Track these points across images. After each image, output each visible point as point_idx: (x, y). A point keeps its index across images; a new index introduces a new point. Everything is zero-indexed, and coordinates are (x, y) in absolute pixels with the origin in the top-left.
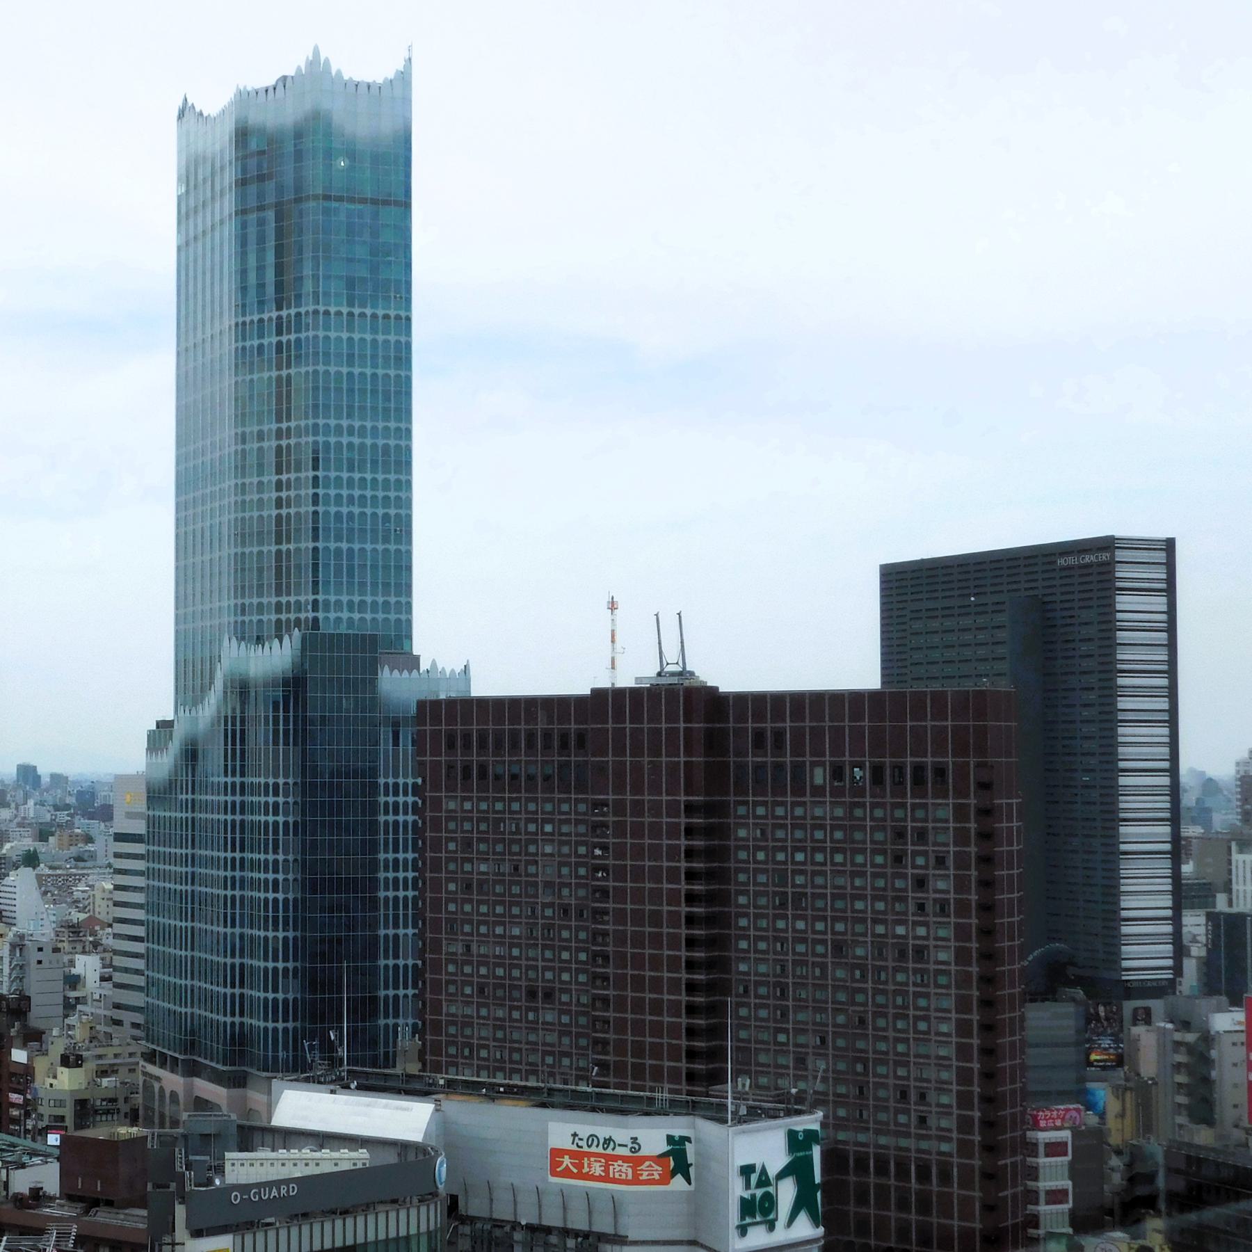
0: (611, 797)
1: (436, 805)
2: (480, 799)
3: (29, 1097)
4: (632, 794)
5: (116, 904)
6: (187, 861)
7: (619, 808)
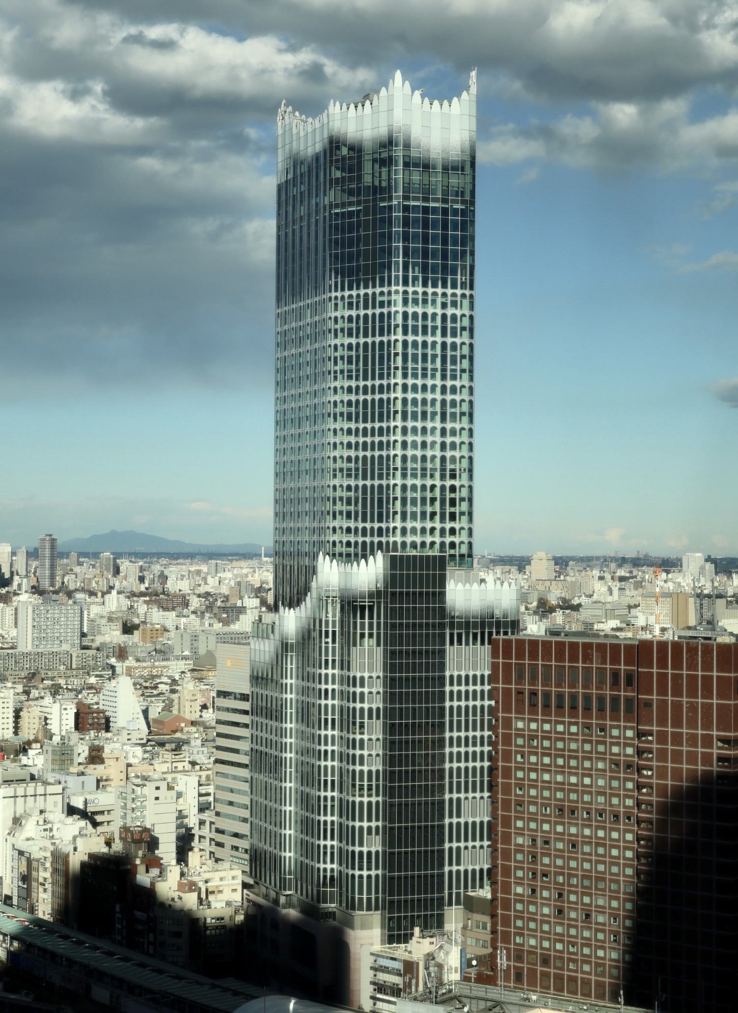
0: (655, 728)
1: (508, 723)
2: (544, 721)
3: (151, 915)
4: (672, 727)
5: (219, 748)
6: (325, 853)
7: (662, 737)
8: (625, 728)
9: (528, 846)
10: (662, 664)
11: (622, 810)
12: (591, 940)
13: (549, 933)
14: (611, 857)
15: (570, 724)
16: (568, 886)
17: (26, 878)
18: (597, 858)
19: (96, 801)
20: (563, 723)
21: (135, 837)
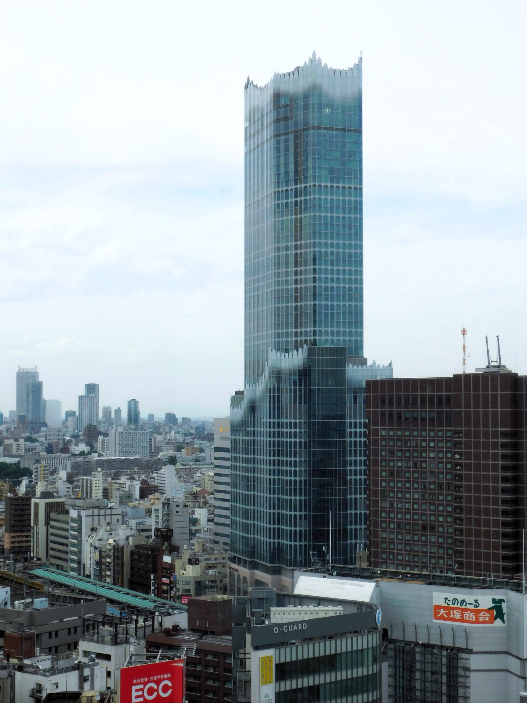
0: (463, 429)
1: (376, 432)
3: (172, 580)
9: (389, 508)
10: (467, 389)
11: (445, 481)
13: (402, 560)
14: (439, 511)
16: (413, 531)
17: (98, 563)
19: (144, 523)
21: (164, 534)
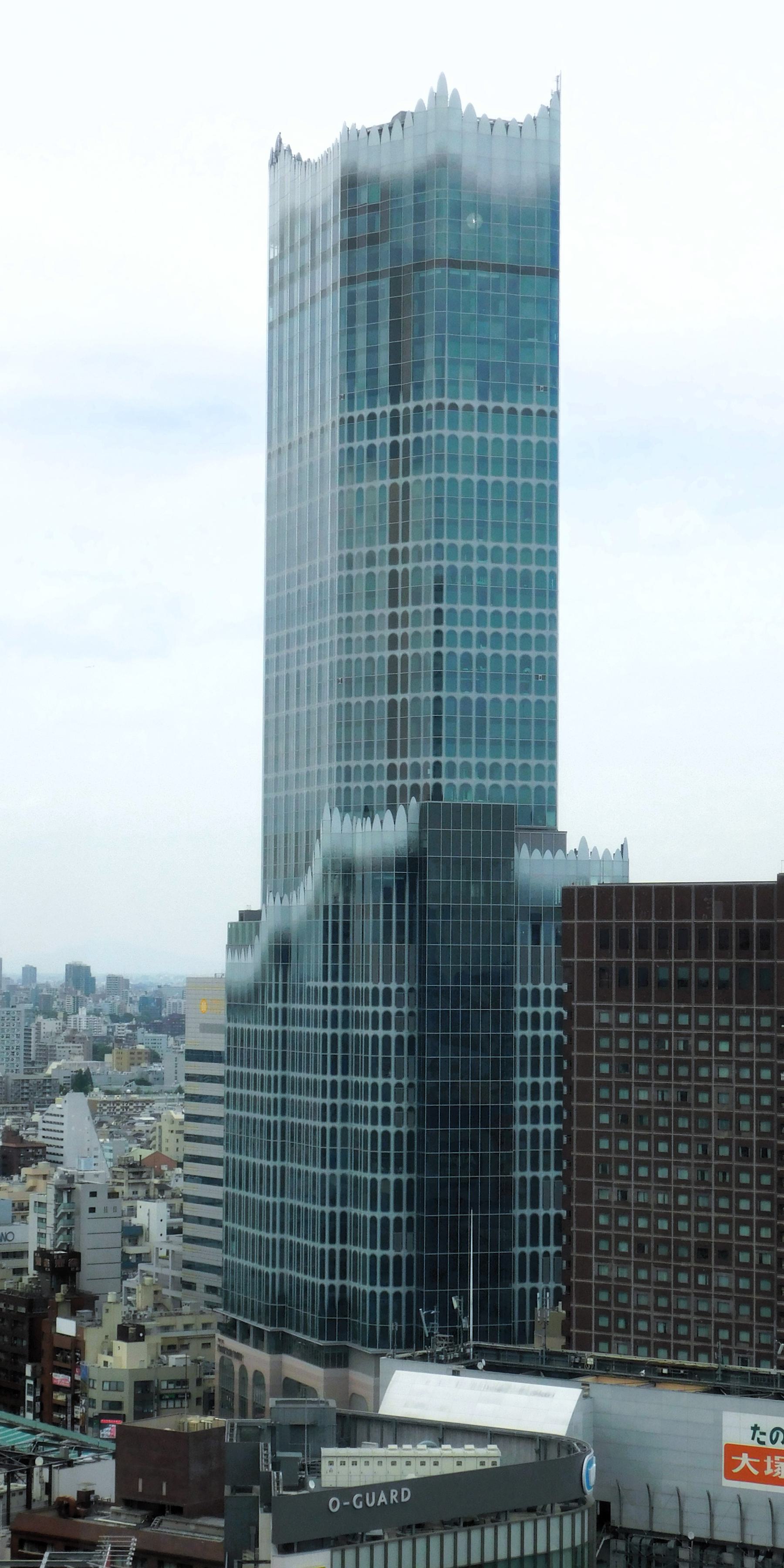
1: (586, 1016)
3: (77, 1377)
8: (760, 1014)
11: (755, 1139)
12: (710, 1341)
14: (739, 1212)
15: (678, 1011)
18: (717, 1215)
19: (10, 1237)
20: (668, 1011)
